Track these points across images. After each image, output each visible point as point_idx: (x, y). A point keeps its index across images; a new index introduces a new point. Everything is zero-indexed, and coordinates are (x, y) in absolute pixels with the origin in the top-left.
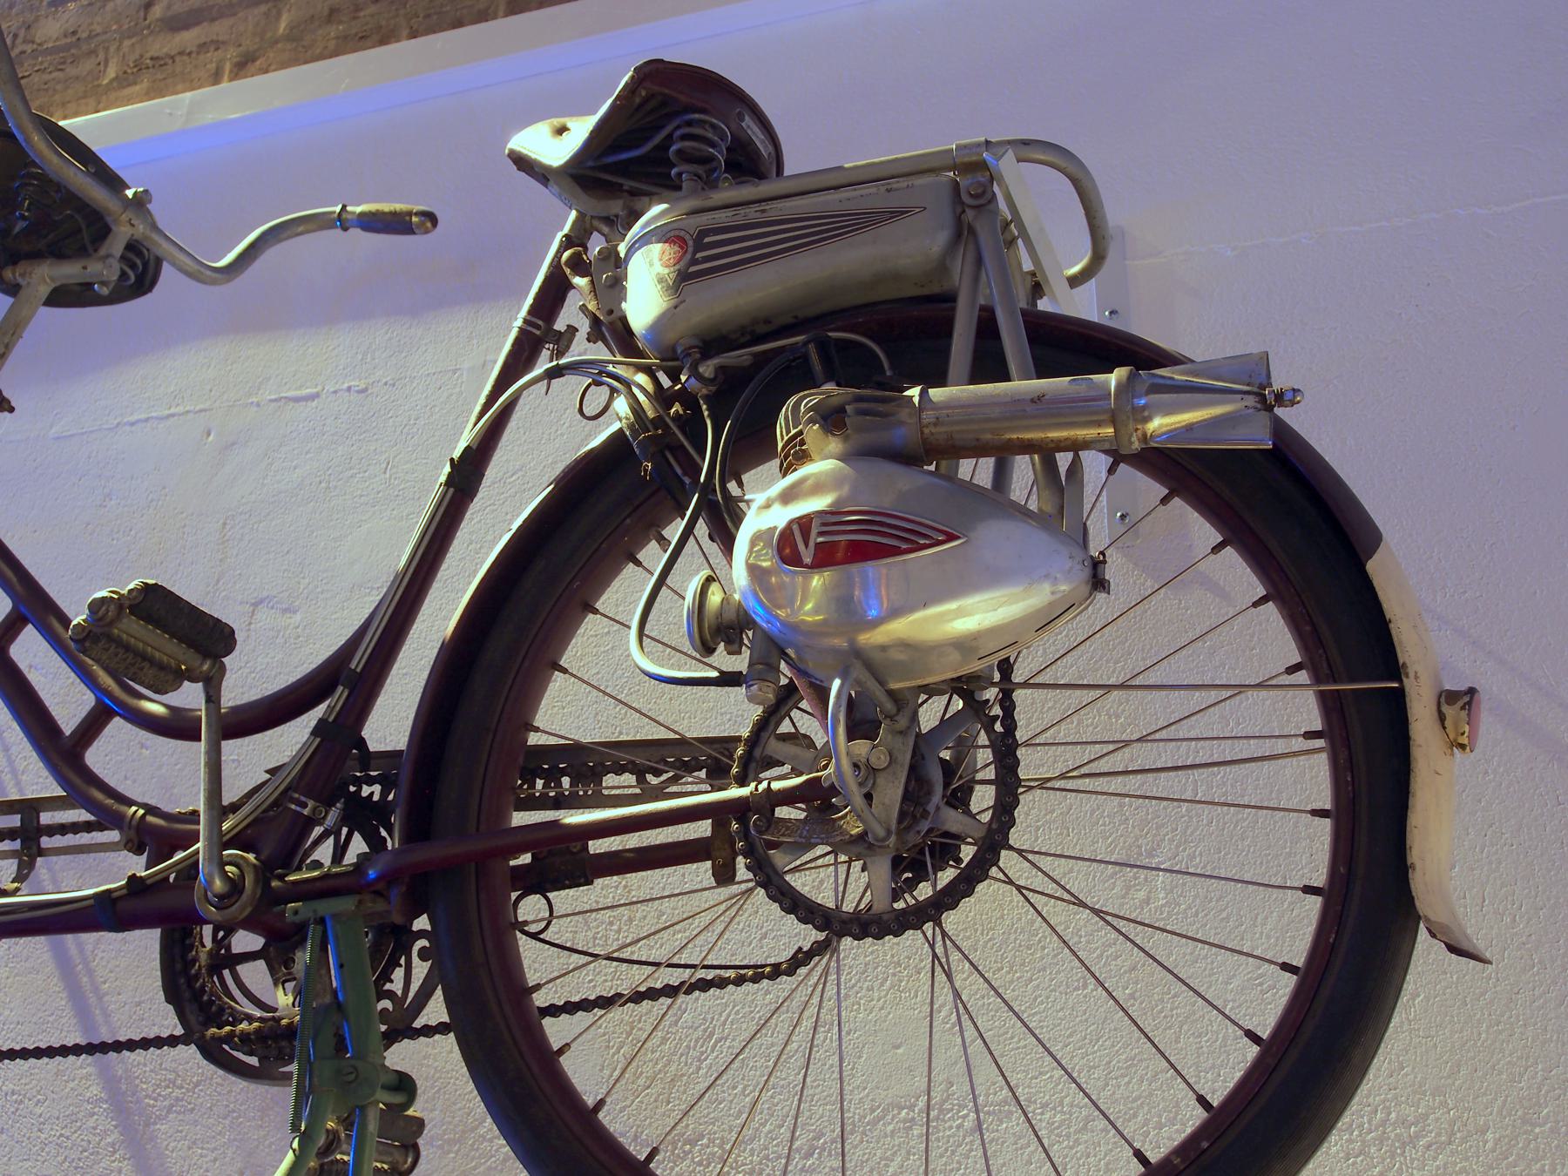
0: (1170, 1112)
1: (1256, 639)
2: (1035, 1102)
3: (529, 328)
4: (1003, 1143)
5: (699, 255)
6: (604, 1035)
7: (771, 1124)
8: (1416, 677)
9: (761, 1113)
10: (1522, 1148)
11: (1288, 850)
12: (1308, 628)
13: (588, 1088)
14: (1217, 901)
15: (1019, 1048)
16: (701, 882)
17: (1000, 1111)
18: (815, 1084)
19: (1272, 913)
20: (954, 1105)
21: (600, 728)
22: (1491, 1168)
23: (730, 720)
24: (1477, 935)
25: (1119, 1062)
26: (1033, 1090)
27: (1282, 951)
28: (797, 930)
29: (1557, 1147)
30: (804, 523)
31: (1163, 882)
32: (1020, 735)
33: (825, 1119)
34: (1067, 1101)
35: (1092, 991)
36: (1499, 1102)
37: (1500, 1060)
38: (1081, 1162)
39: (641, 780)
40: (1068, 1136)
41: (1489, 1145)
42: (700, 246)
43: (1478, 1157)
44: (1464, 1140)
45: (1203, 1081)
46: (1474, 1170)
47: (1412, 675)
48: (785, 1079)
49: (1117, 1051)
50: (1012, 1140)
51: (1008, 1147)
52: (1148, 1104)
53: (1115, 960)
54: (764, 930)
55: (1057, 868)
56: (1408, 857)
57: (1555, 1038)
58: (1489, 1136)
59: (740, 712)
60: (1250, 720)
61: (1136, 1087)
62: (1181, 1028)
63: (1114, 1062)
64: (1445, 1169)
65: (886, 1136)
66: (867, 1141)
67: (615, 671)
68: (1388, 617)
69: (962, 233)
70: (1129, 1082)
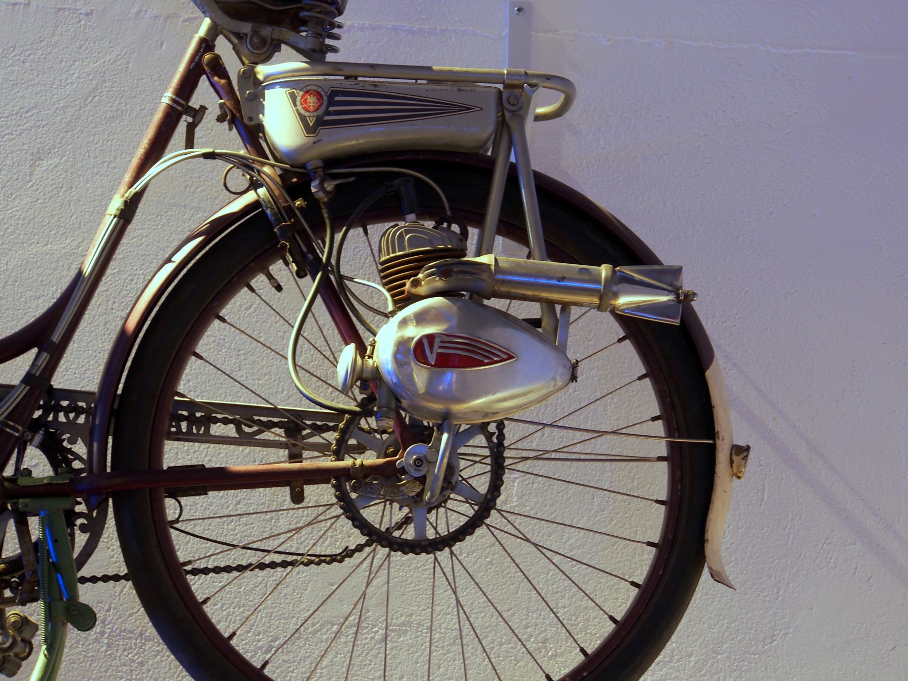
0: (508, 636)
1: (592, 334)
2: (423, 625)
3: (175, 105)
4: (401, 649)
5: (331, 109)
6: (116, 562)
7: (242, 630)
8: (723, 440)
9: (234, 623)
10: (709, 667)
11: (597, 478)
12: (668, 400)
13: (104, 598)
14: (550, 506)
15: (414, 591)
16: (191, 459)
17: (399, 630)
18: (274, 606)
19: (583, 517)
20: (369, 624)
21: (109, 334)
22: (691, 677)
23: (214, 342)
24: (730, 571)
25: (479, 603)
26: (422, 618)
27: (587, 541)
28: (263, 501)
29: (729, 666)
30: (431, 338)
31: (517, 491)
32: (506, 443)
33: (280, 628)
34: (444, 625)
35: (465, 557)
36: (701, 640)
37: (704, 616)
38: (450, 663)
39: (239, 430)
40: (443, 647)
41: (692, 664)
42: (332, 103)
43: (685, 670)
44: (679, 660)
45: (530, 618)
46: (681, 678)
47: (721, 438)
48: (252, 601)
49: (479, 596)
50: (406, 648)
51: (403, 652)
52: (495, 630)
53: (481, 538)
54: (238, 498)
55: (518, 520)
56: (706, 535)
57: (736, 605)
58: (693, 659)
59: (222, 337)
60: (583, 389)
61: (488, 619)
62: (520, 585)
63: (476, 603)
64: (666, 676)
65: (322, 642)
66: (309, 644)
67: (121, 291)
68: (713, 405)
69: (502, 126)
70: (484, 616)
